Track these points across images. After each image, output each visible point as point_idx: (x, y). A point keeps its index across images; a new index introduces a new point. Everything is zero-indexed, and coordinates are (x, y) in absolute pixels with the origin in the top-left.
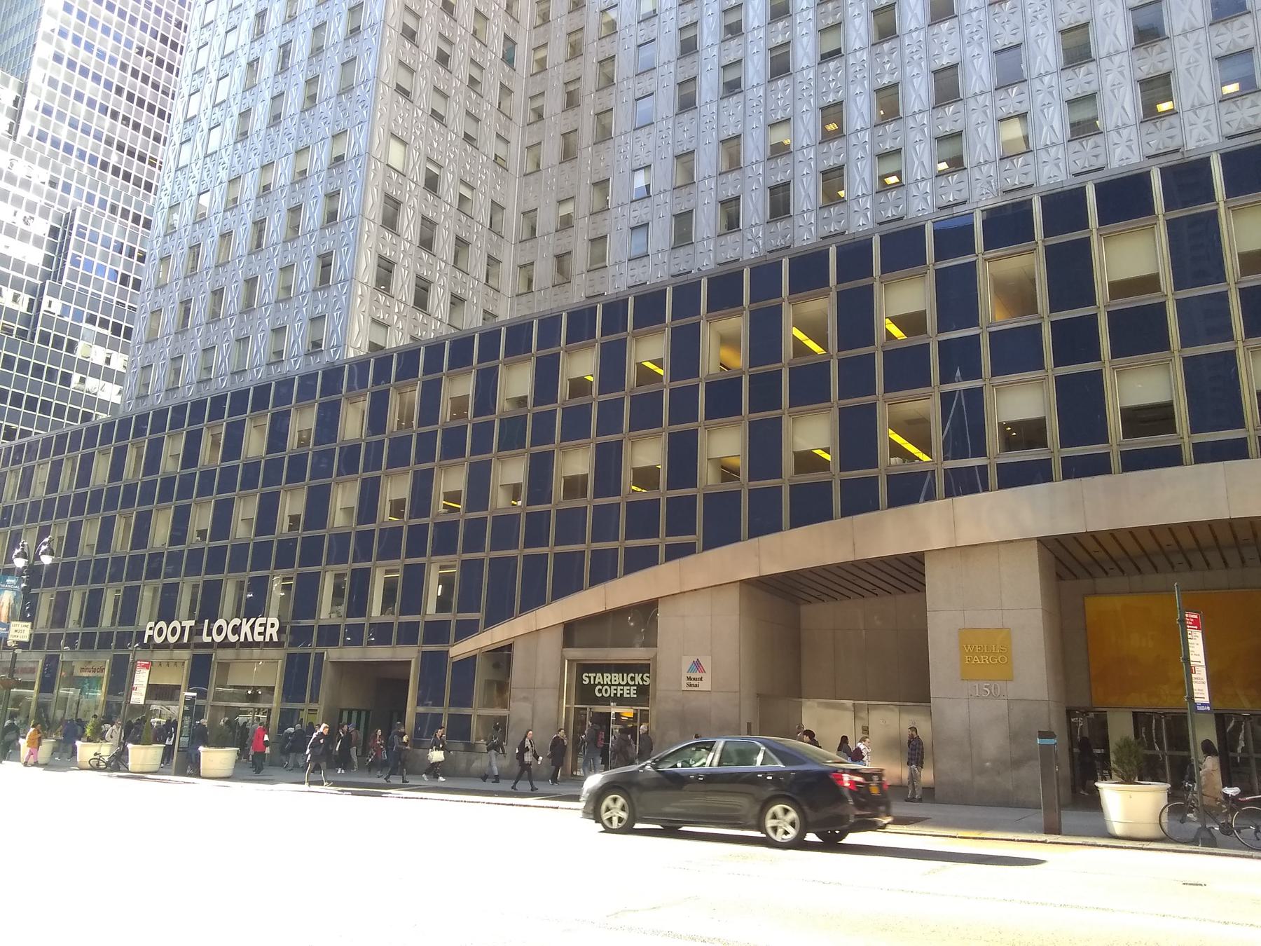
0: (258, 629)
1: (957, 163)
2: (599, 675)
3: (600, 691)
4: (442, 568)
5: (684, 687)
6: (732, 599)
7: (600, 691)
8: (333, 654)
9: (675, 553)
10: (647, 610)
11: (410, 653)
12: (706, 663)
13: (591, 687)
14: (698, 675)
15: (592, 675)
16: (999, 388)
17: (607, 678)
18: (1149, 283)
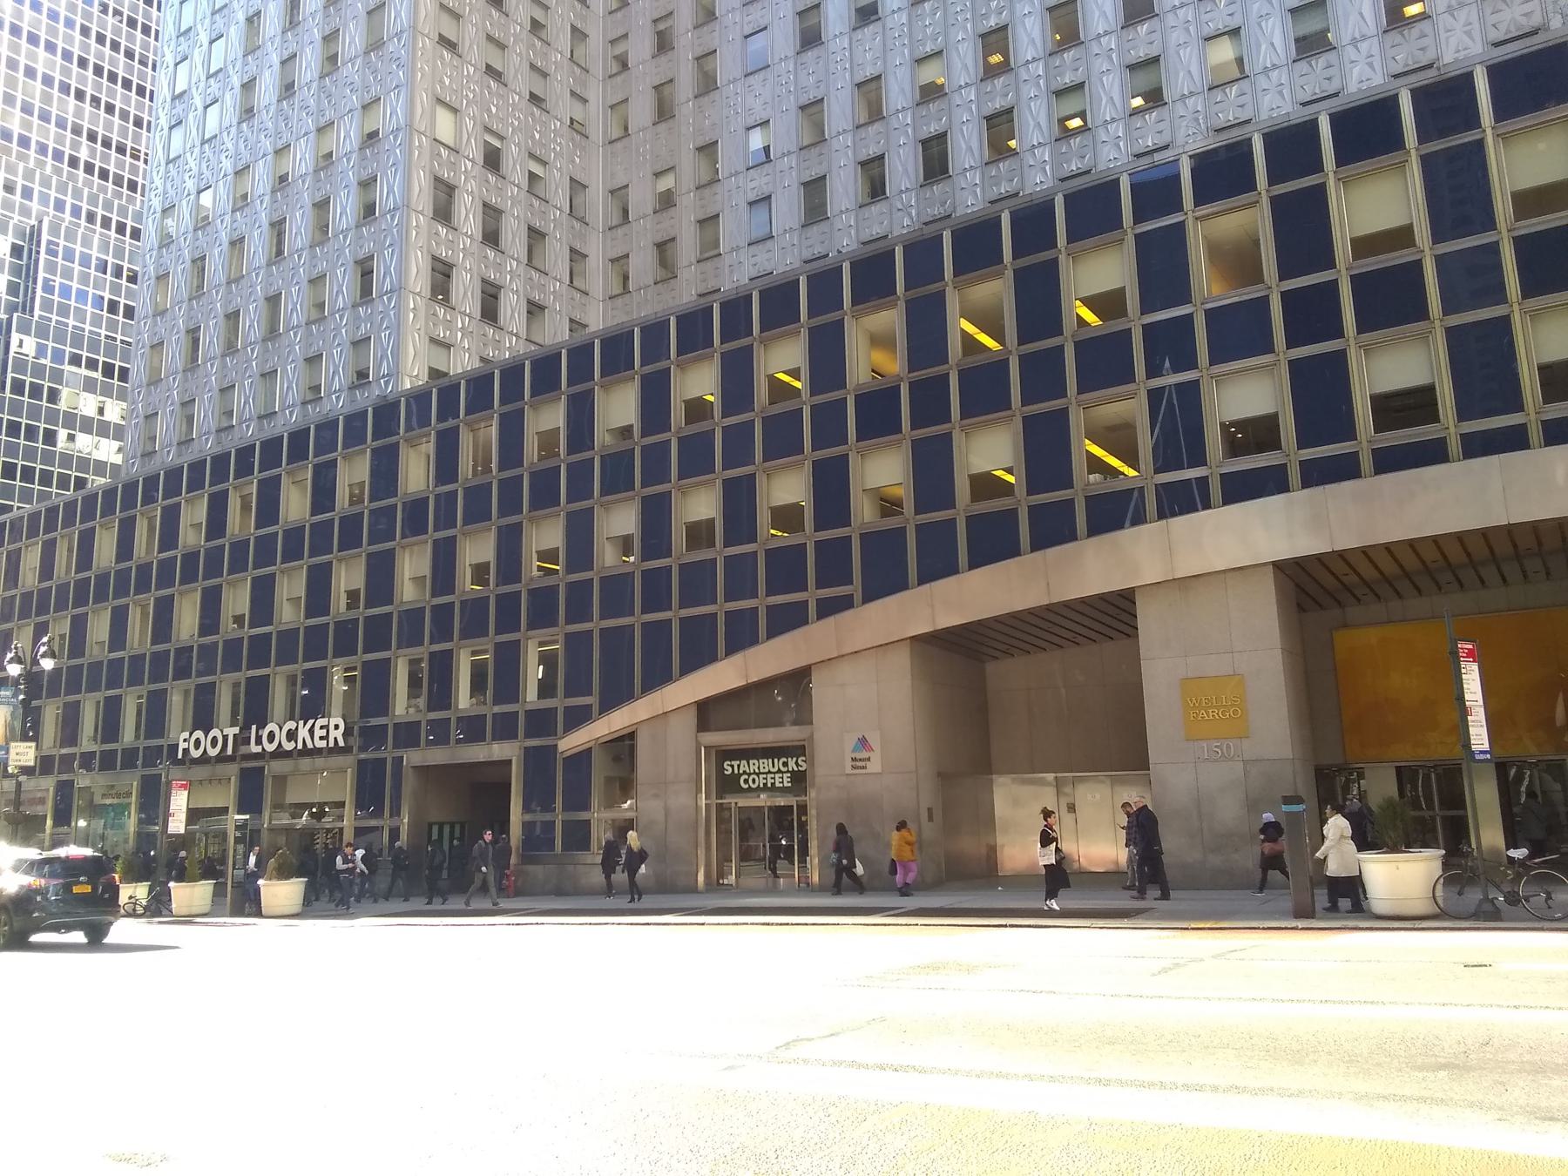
0: (318, 733)
1: (1155, 98)
2: (744, 762)
3: (746, 781)
4: (541, 644)
5: (849, 770)
6: (902, 660)
7: (746, 781)
8: (412, 757)
9: (828, 608)
10: (797, 681)
11: (499, 750)
12: (874, 740)
13: (735, 778)
14: (864, 755)
15: (735, 763)
16: (1219, 380)
17: (754, 765)
18: (1401, 237)
